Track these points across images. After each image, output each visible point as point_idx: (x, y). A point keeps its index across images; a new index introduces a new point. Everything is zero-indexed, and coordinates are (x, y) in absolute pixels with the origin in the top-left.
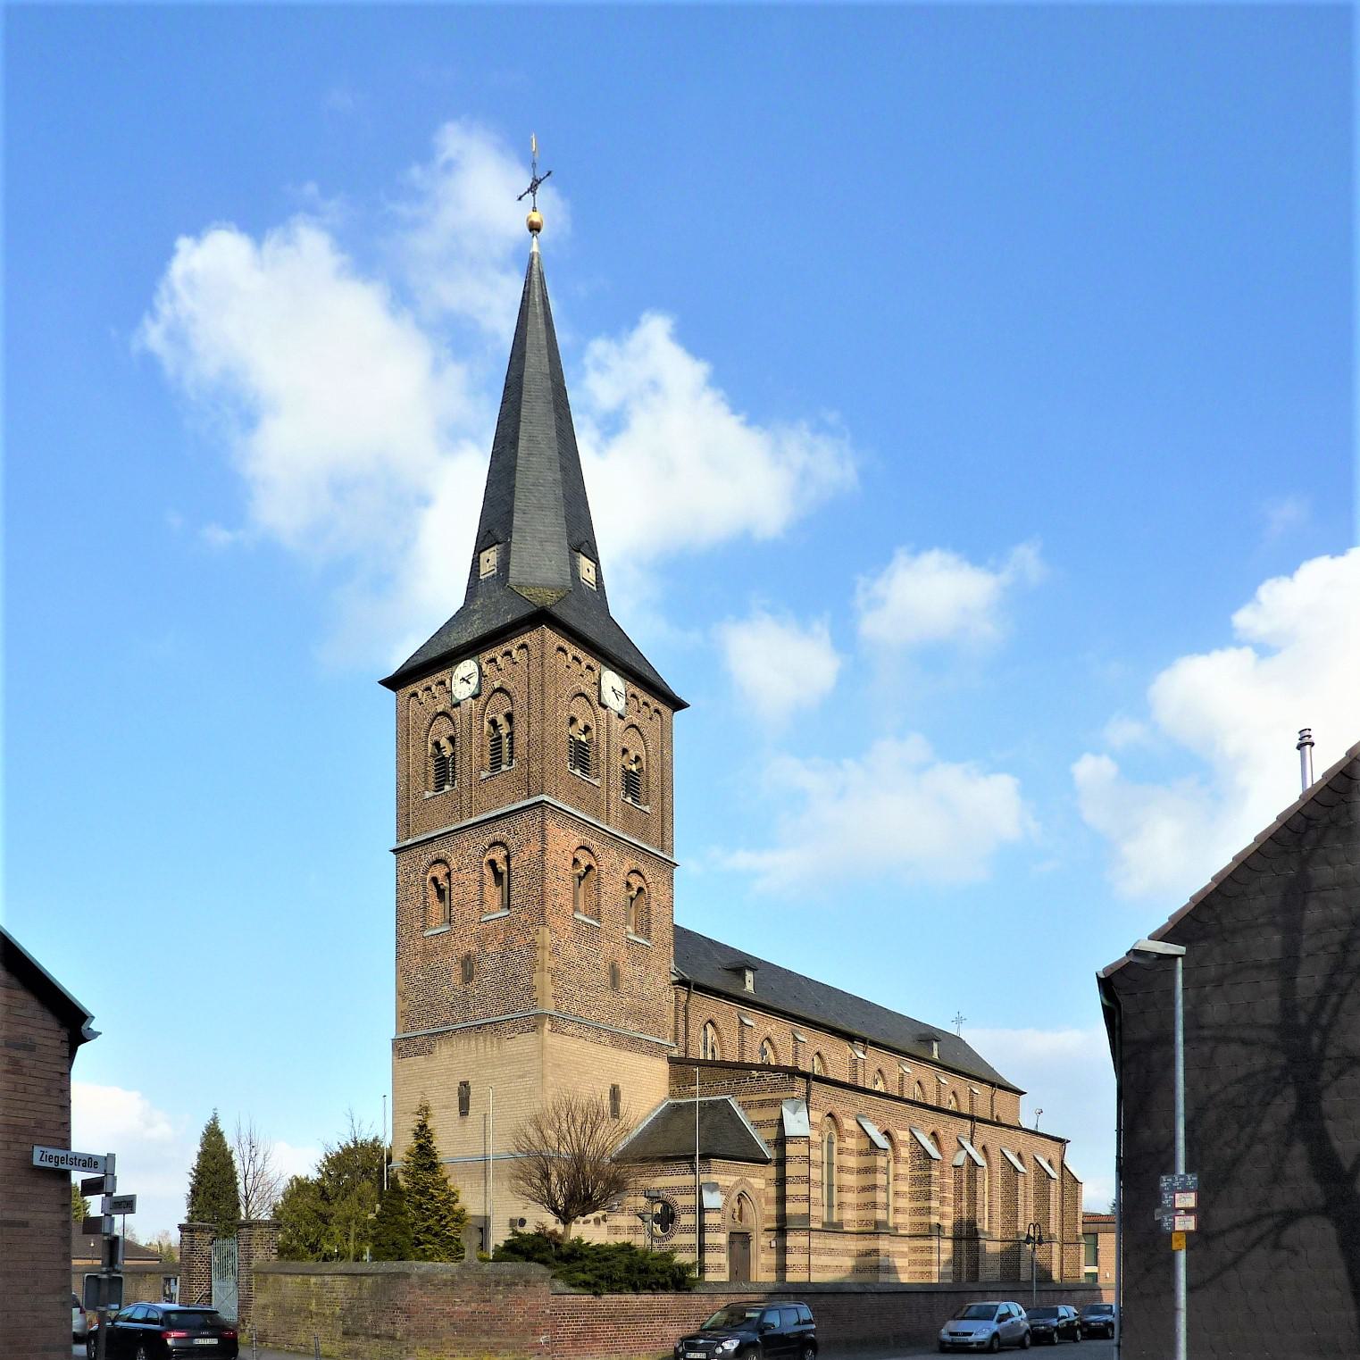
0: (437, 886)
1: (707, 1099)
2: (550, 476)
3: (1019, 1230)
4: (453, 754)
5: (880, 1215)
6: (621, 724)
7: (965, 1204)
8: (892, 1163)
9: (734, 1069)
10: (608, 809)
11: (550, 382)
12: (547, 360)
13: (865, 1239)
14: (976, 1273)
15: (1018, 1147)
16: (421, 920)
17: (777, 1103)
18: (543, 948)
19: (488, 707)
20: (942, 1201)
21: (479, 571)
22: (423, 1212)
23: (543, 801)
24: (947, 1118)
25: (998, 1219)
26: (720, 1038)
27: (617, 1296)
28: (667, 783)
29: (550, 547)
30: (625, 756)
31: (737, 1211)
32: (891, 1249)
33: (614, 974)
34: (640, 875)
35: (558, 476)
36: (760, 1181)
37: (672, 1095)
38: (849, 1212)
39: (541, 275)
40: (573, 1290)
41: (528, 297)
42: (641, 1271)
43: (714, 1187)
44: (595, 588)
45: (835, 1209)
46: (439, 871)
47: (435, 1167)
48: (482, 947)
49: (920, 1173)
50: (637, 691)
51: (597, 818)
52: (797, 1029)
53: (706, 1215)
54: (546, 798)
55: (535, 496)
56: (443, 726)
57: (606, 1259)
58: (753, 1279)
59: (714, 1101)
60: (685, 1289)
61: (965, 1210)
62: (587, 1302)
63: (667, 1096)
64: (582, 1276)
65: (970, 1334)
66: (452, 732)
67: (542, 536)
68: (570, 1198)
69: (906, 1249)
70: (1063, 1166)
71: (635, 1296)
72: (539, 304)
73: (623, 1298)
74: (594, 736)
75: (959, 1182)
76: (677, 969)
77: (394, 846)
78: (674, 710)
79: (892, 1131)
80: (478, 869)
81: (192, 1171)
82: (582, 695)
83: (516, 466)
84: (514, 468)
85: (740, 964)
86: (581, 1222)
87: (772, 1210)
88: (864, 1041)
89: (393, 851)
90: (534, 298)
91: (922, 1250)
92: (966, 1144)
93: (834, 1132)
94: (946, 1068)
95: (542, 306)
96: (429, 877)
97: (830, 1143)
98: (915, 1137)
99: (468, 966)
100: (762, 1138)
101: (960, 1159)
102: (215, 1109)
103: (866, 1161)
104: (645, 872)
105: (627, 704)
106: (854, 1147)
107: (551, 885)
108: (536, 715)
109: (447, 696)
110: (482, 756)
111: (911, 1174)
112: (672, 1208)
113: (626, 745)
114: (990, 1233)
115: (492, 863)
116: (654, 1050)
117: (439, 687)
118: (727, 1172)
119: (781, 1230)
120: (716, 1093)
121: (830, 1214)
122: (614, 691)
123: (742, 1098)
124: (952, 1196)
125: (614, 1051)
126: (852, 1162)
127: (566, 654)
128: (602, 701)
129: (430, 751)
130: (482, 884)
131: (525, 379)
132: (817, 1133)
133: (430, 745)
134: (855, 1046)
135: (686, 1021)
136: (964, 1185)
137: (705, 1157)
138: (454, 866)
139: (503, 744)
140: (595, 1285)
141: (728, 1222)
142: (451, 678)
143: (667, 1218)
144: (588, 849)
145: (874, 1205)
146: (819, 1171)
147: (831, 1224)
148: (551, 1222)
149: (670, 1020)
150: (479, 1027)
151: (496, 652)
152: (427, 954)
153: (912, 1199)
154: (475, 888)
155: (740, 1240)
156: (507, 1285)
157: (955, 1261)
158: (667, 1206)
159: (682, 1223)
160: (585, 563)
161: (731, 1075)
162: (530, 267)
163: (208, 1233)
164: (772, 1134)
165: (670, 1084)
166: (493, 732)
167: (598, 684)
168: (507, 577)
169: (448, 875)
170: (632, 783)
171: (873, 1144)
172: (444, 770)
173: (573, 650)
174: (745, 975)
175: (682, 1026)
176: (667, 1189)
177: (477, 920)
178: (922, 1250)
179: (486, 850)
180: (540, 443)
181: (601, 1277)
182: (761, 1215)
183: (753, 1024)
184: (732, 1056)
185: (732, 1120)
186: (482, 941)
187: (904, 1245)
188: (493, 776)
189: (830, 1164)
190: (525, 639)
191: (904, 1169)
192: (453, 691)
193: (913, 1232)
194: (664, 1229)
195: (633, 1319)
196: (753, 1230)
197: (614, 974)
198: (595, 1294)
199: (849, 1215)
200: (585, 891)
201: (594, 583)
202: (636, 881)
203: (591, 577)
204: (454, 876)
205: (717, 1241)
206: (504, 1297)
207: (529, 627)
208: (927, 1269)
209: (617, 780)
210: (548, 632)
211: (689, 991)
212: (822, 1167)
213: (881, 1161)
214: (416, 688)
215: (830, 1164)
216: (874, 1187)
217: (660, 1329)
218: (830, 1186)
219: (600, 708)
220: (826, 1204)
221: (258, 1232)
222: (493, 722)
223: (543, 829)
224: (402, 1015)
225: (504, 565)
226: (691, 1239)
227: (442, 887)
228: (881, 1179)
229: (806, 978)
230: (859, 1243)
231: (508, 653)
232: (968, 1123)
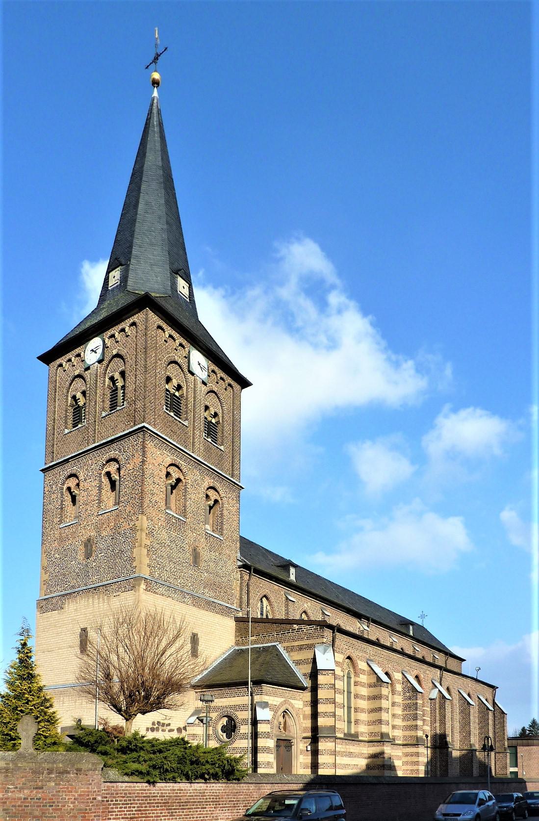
0: (71, 493)
1: (262, 645)
2: (159, 226)
3: (471, 743)
4: (85, 404)
5: (385, 729)
6: (205, 389)
7: (438, 724)
8: (390, 694)
9: (281, 624)
10: (193, 443)
11: (162, 172)
12: (160, 158)
13: (374, 746)
14: (446, 771)
15: (469, 689)
16: (59, 516)
17: (311, 647)
18: (141, 530)
19: (109, 368)
21: (108, 285)
23: (144, 427)
24: (425, 667)
27: (171, 785)
28: (236, 433)
29: (157, 269)
30: (207, 412)
31: (282, 723)
32: (392, 754)
33: (196, 556)
34: (216, 491)
36: (300, 702)
37: (237, 644)
40: (126, 778)
41: (150, 121)
42: (192, 763)
43: (265, 705)
44: (188, 300)
45: (353, 724)
46: (72, 483)
47: (32, 677)
49: (409, 702)
50: (216, 369)
51: (186, 447)
54: (147, 425)
56: (79, 384)
57: (160, 751)
58: (294, 772)
59: (266, 647)
60: (235, 779)
61: (438, 729)
62: (141, 790)
63: (233, 644)
64: (135, 766)
65: (459, 815)
66: (84, 388)
67: (152, 261)
69: (401, 754)
70: (494, 704)
71: (188, 785)
72: (157, 126)
73: (176, 786)
74: (185, 394)
75: (433, 711)
76: (242, 558)
78: (243, 388)
79: (390, 672)
80: (98, 479)
82: (176, 363)
83: (136, 219)
84: (135, 220)
86: (167, 730)
87: (308, 723)
88: (368, 619)
89: (42, 471)
90: (153, 122)
92: (438, 685)
94: (418, 641)
96: (65, 487)
97: (349, 678)
98: (406, 677)
99: (88, 544)
100: (301, 673)
101: (434, 694)
103: (374, 691)
105: (209, 376)
106: (365, 681)
107: (149, 487)
108: (140, 368)
110: (103, 401)
111: (404, 702)
112: (234, 721)
113: (208, 404)
115: (108, 474)
116: (225, 611)
117: (77, 358)
119: (315, 739)
121: (349, 727)
122: (199, 364)
123: (286, 644)
124: (429, 719)
125: (195, 609)
126: (364, 691)
127: (164, 332)
129: (69, 402)
130: (100, 488)
132: (340, 669)
134: (362, 622)
135: (248, 594)
136: (437, 711)
137: (257, 683)
138: (81, 477)
139: (118, 398)
140: (148, 773)
141: (275, 731)
143: (231, 728)
144: (178, 467)
145: (380, 722)
148: (116, 720)
150: (95, 588)
151: (115, 330)
153: (404, 719)
154: (95, 491)
155: (284, 745)
156: (59, 773)
157: (431, 764)
158: (231, 719)
159: (241, 731)
160: (181, 283)
161: (278, 629)
162: (152, 105)
164: (308, 669)
165: (236, 636)
167: (188, 357)
168: (125, 286)
169: (78, 485)
170: (211, 430)
172: (78, 413)
173: (169, 331)
174: (289, 570)
175: (245, 598)
177: (96, 514)
179: (104, 465)
180: (153, 207)
181: (154, 767)
182: (300, 727)
184: (281, 615)
186: (98, 528)
187: (400, 751)
188: (111, 414)
189: (349, 693)
191: (399, 699)
192: (86, 360)
193: (405, 742)
194: (229, 736)
195: (184, 804)
196: (294, 738)
197: (196, 556)
198: (148, 782)
199: (363, 729)
201: (187, 297)
202: (213, 495)
203: (186, 292)
204: (81, 484)
205: (267, 745)
206: (56, 784)
207: (137, 309)
208: (415, 767)
210: (151, 314)
211: (250, 574)
212: (344, 694)
213: (385, 691)
214: (62, 360)
215: (349, 693)
216: (380, 709)
217: (212, 814)
218: (349, 708)
219: (189, 375)
220: (346, 720)
222: (112, 379)
223: (144, 447)
225: (124, 279)
230: (369, 749)
231: (123, 330)
232: (438, 671)
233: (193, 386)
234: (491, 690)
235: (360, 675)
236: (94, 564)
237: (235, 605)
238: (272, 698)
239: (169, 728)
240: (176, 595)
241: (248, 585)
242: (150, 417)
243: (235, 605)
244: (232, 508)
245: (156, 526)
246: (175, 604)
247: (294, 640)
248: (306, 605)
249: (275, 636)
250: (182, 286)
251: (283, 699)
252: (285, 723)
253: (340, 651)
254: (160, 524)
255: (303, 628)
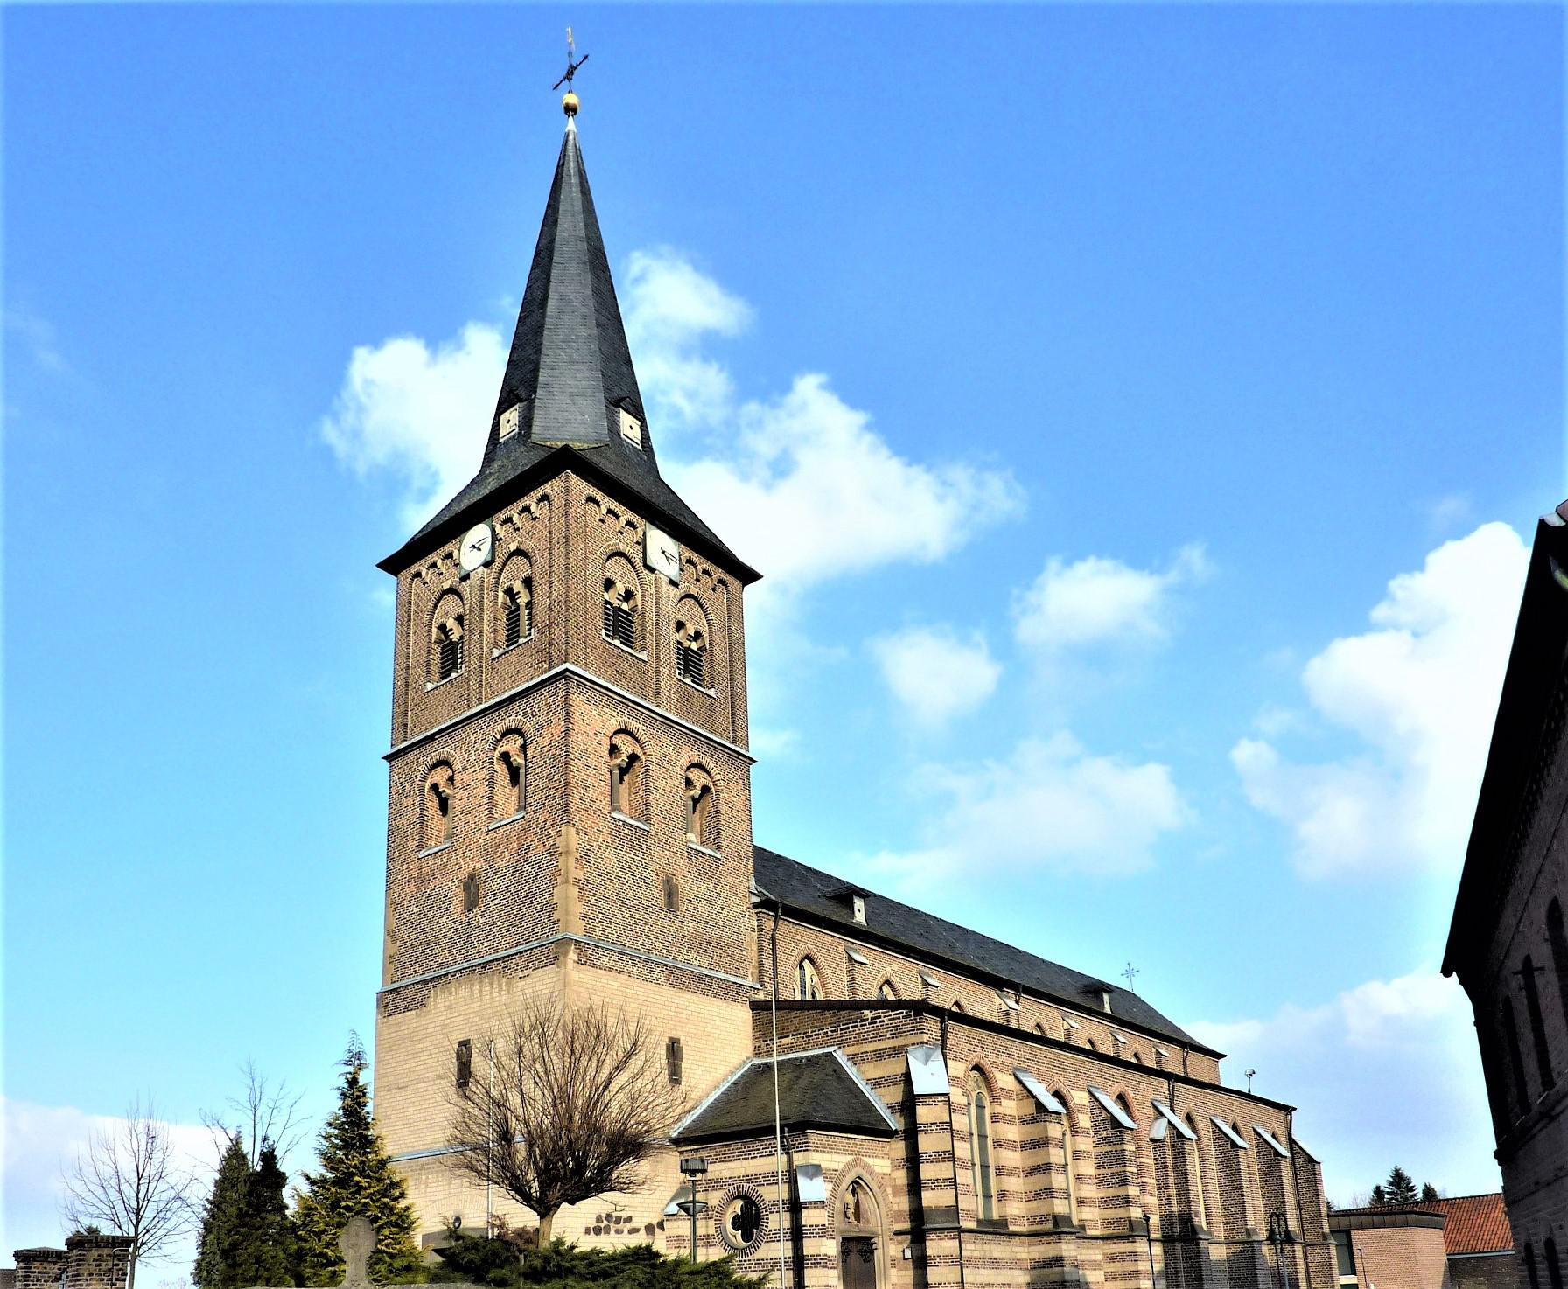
0: (438, 794)
4: (462, 637)
5: (1060, 1207)
6: (675, 593)
7: (1173, 1192)
8: (1068, 1136)
9: (840, 1009)
15: (1233, 1116)
17: (901, 1051)
18: (567, 853)
19: (503, 574)
20: (1143, 1186)
21: (499, 434)
22: (340, 1214)
23: (567, 670)
25: (1218, 1214)
26: (822, 979)
28: (737, 665)
29: (582, 402)
30: (682, 631)
31: (852, 1206)
34: (704, 770)
35: (595, 331)
37: (757, 1054)
38: (1015, 1204)
39: (578, 150)
43: (815, 1171)
44: (640, 448)
45: (995, 1200)
48: (490, 862)
49: (1108, 1148)
52: (925, 970)
53: (805, 1213)
55: (566, 352)
59: (813, 1056)
66: (460, 611)
68: (548, 1176)
69: (1100, 1257)
70: (1292, 1143)
74: (639, 604)
75: (1161, 1164)
76: (759, 888)
77: (389, 751)
78: (744, 585)
79: (1064, 1092)
80: (488, 766)
81: (206, 1203)
82: (621, 554)
85: (846, 894)
87: (903, 1203)
91: (1123, 1258)
92: (1166, 1110)
93: (984, 1091)
95: (578, 177)
96: (427, 785)
97: (980, 1107)
99: (472, 888)
100: (882, 1102)
101: (1160, 1130)
102: (239, 1127)
103: (1032, 1131)
104: (711, 766)
105: (682, 570)
106: (1014, 1112)
107: (578, 774)
109: (454, 570)
110: (495, 631)
111: (1098, 1150)
112: (756, 1206)
113: (682, 618)
114: (1210, 1233)
115: (505, 757)
116: (730, 991)
118: (833, 1150)
120: (817, 1045)
121: (988, 1207)
122: (664, 552)
124: (1154, 1181)
125: (671, 991)
127: (599, 505)
128: (648, 563)
129: (434, 636)
130: (491, 783)
131: (557, 244)
132: (960, 1091)
133: (434, 630)
135: (774, 949)
136: (1170, 1164)
141: (839, 1222)
142: (460, 547)
145: (1049, 1192)
146: (970, 1173)
147: (991, 1222)
148: (522, 1217)
149: (751, 954)
150: (484, 965)
151: (513, 511)
152: (422, 879)
154: (483, 789)
158: (749, 1202)
161: (834, 1020)
163: (55, 1263)
164: (896, 1094)
165: (755, 1038)
166: (510, 604)
167: (643, 543)
168: (529, 434)
169: (451, 779)
170: (690, 662)
171: (1040, 1107)
172: (450, 655)
173: (607, 502)
175: (768, 962)
176: (748, 1178)
178: (1123, 1258)
179: (497, 741)
183: (867, 962)
184: (839, 993)
185: (839, 1078)
186: (490, 855)
187: (1097, 1251)
188: (508, 652)
189: (983, 1137)
190: (546, 488)
191: (1086, 1144)
193: (1106, 1232)
194: (747, 1237)
196: (877, 1235)
197: (671, 894)
199: (1015, 1209)
200: (629, 789)
201: (639, 442)
203: (636, 434)
204: (457, 778)
205: (823, 1251)
209: (671, 656)
210: (575, 480)
212: (971, 1139)
213: (1054, 1130)
215: (983, 1137)
216: (1047, 1167)
220: (980, 1192)
221: (94, 1254)
222: (509, 592)
223: (567, 706)
224: (391, 960)
225: (526, 423)
226: (785, 1249)
227: (443, 795)
228: (1056, 1156)
229: (936, 918)
231: (526, 509)
233: (653, 591)
234: (1282, 1114)
235: (1003, 1100)
236: (481, 921)
237: (750, 978)
238: (827, 1156)
239: (629, 1226)
240: (636, 968)
241: (773, 939)
242: (578, 651)
243: (750, 978)
244: (735, 799)
245: (595, 844)
246: (636, 984)
247: (866, 1041)
248: (888, 969)
249: (830, 1033)
250: (628, 424)
251: (850, 1158)
252: (857, 1204)
253: (959, 1055)
254: (601, 840)
255: (882, 1015)
